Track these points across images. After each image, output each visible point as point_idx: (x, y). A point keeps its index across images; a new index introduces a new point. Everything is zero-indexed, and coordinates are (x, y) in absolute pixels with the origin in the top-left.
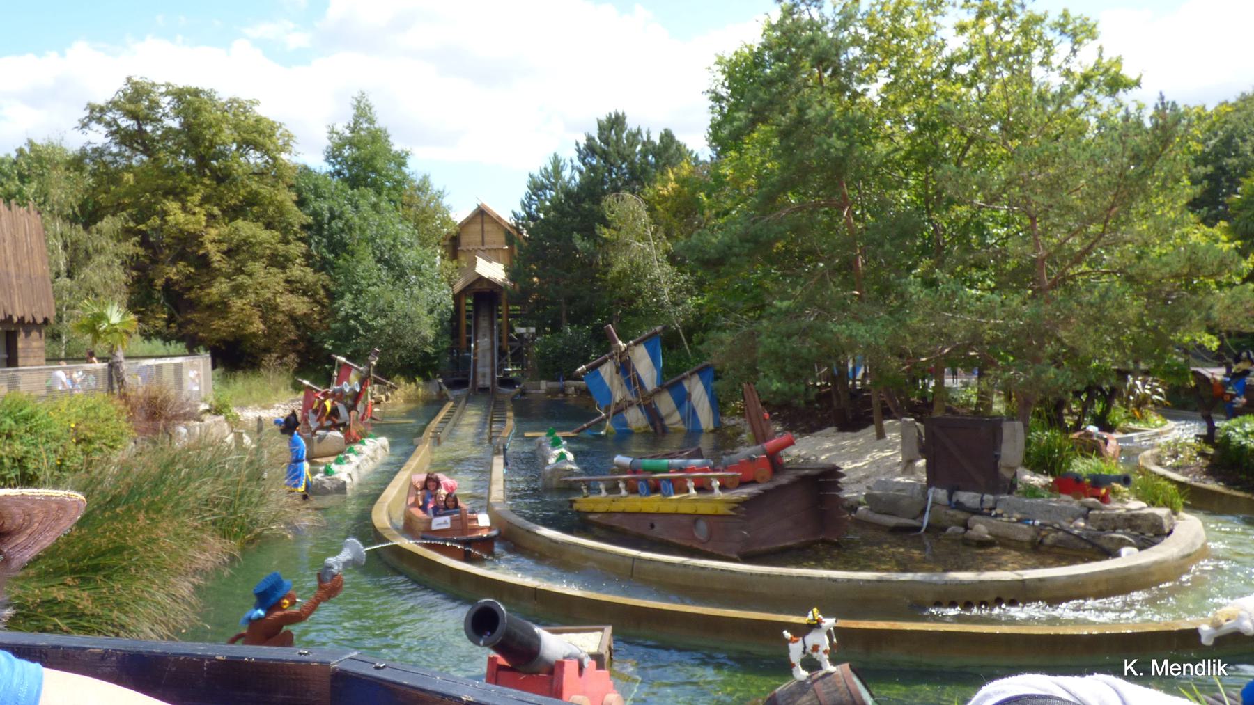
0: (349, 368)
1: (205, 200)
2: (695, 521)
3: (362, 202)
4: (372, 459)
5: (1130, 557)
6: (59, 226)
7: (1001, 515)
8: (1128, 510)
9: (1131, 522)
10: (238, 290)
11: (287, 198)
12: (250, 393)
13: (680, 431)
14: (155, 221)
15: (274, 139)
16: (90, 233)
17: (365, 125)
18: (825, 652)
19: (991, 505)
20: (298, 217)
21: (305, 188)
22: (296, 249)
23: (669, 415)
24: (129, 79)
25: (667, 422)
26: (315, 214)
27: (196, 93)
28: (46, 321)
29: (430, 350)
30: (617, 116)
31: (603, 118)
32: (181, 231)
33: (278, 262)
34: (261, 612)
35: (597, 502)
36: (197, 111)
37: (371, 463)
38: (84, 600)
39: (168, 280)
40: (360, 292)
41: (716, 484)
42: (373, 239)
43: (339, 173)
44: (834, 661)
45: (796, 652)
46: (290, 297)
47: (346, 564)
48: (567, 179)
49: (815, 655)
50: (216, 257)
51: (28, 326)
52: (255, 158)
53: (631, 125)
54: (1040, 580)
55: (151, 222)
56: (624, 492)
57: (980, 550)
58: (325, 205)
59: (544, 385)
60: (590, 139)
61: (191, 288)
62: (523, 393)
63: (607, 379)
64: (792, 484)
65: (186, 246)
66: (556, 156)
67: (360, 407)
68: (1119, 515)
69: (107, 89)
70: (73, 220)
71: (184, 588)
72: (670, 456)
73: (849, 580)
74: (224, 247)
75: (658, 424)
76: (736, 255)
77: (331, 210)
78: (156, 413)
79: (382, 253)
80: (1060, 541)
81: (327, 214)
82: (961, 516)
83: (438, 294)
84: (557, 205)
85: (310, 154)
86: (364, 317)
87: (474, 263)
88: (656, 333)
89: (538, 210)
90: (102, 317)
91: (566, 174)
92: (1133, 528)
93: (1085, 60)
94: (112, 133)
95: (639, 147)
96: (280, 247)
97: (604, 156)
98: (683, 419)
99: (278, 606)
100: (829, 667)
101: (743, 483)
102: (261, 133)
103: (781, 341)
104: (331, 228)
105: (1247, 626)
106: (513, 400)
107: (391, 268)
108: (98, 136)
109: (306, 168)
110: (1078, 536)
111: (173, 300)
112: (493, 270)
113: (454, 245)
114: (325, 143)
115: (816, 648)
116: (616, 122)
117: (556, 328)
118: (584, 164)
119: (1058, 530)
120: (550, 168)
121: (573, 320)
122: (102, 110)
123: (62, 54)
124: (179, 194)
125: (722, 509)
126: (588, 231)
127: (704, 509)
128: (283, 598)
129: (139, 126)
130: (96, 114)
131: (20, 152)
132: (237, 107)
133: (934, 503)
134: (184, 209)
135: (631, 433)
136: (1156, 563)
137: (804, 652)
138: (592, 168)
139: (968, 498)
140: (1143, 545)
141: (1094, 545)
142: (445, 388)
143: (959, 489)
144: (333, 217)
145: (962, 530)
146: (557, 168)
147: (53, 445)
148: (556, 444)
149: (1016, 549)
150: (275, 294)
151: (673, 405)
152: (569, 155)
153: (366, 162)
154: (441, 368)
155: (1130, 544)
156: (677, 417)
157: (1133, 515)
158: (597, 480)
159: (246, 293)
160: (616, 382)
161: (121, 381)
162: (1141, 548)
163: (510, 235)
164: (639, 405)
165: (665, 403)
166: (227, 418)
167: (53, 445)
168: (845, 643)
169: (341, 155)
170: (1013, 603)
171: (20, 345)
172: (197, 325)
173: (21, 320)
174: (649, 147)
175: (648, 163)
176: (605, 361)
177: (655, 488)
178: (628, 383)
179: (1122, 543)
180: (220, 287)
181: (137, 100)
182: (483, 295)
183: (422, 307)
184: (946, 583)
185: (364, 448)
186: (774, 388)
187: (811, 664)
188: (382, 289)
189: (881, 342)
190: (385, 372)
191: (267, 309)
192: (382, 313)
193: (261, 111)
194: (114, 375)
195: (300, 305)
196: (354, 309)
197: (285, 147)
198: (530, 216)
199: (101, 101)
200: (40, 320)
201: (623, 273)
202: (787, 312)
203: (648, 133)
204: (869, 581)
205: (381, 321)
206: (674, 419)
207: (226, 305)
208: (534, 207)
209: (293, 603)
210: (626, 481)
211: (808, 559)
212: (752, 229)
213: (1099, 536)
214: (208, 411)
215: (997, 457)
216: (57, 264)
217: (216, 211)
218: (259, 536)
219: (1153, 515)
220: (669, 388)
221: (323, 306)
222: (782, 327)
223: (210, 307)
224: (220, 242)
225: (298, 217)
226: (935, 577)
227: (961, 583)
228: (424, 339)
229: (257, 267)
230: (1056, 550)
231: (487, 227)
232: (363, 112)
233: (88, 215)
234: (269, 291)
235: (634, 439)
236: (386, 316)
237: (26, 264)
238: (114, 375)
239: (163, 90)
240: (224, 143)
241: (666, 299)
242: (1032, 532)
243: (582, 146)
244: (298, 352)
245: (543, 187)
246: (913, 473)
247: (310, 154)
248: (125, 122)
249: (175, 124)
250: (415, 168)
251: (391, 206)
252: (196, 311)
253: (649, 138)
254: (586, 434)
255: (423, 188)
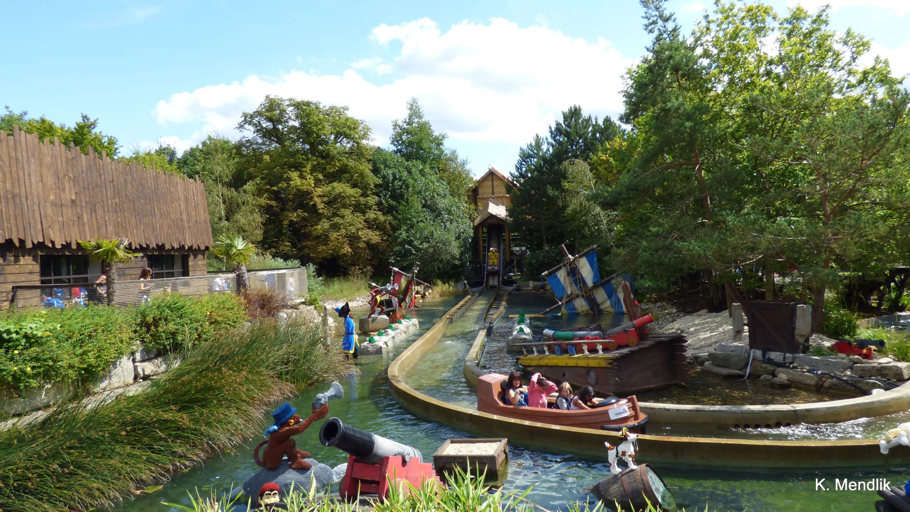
0: (401, 275)
1: (313, 170)
2: (588, 372)
3: (413, 170)
4: (405, 332)
5: (878, 395)
6: (220, 189)
7: (796, 367)
8: (880, 364)
9: (882, 372)
10: (336, 227)
11: (366, 168)
12: (342, 291)
13: (610, 313)
14: (283, 185)
15: (357, 130)
16: (239, 193)
17: (416, 120)
18: (630, 456)
19: (790, 360)
20: (373, 180)
21: (377, 160)
22: (372, 200)
23: (603, 303)
24: (267, 97)
25: (602, 307)
26: (384, 177)
27: (308, 104)
28: (207, 248)
29: (457, 262)
30: (576, 109)
31: (566, 110)
32: (299, 190)
33: (360, 208)
34: (275, 427)
35: (531, 359)
36: (308, 115)
37: (404, 335)
38: (184, 419)
39: (291, 221)
40: (412, 227)
41: (600, 347)
42: (420, 192)
43: (400, 151)
44: (637, 462)
45: (612, 455)
46: (370, 232)
47: (330, 398)
48: (545, 150)
49: (624, 458)
50: (320, 206)
51: (196, 252)
52: (347, 145)
53: (585, 114)
54: (807, 410)
55: (280, 185)
56: (547, 353)
57: (785, 390)
58: (390, 172)
59: (531, 284)
60: (558, 124)
61: (306, 226)
62: (518, 289)
63: (562, 280)
64: (651, 347)
65: (302, 199)
66: (537, 136)
67: (408, 300)
68: (873, 367)
69: (255, 103)
70: (229, 185)
71: (258, 414)
72: (581, 329)
73: (678, 410)
74: (325, 199)
75: (596, 309)
76: (624, 199)
77: (394, 174)
78: (267, 305)
79: (426, 201)
80: (834, 385)
81: (391, 178)
82: (770, 368)
83: (462, 228)
84: (538, 168)
85: (381, 140)
86: (416, 243)
87: (487, 206)
88: (593, 249)
89: (526, 171)
90: (231, 246)
91: (545, 147)
92: (883, 376)
93: (865, 62)
94: (258, 131)
95: (590, 129)
96: (361, 199)
97: (567, 134)
98: (611, 304)
99: (287, 423)
100: (633, 466)
101: (620, 347)
102: (349, 127)
103: (652, 254)
104: (393, 186)
105: (905, 441)
106: (510, 294)
107: (433, 211)
108: (249, 133)
109: (379, 148)
110: (846, 381)
111: (290, 232)
112: (499, 210)
113: (475, 194)
114: (391, 132)
115: (624, 453)
116: (574, 113)
117: (540, 247)
118: (555, 140)
119: (833, 377)
120: (534, 144)
121: (549, 241)
122: (252, 117)
123: (241, 84)
124: (298, 167)
125: (604, 364)
126: (557, 185)
127: (593, 364)
128: (290, 419)
129: (274, 125)
130: (248, 119)
131: (204, 144)
132: (333, 112)
133: (754, 359)
134: (302, 177)
135: (578, 314)
136: (893, 399)
137: (617, 456)
138: (560, 143)
139: (775, 356)
140: (888, 387)
141: (856, 387)
142: (468, 286)
143: (769, 350)
144: (395, 179)
145: (770, 377)
146: (538, 145)
147: (195, 325)
148: (521, 321)
149: (806, 390)
150: (358, 230)
151: (606, 296)
152: (545, 134)
153: (417, 144)
154: (469, 273)
155: (880, 387)
156: (608, 303)
157: (882, 367)
158: (581, 344)
159: (339, 229)
160: (568, 281)
161: (245, 286)
162: (886, 389)
163: (509, 187)
164: (583, 296)
165: (601, 296)
166: (315, 308)
167: (195, 325)
168: (644, 451)
169: (401, 139)
170: (788, 425)
171: (190, 264)
172: (309, 249)
173: (191, 248)
174: (596, 128)
175: (596, 139)
176: (560, 268)
177: (565, 351)
178: (575, 282)
179: (875, 386)
180: (324, 225)
181: (272, 110)
182: (492, 225)
183: (451, 235)
184: (742, 412)
185: (400, 326)
186: (647, 285)
187: (622, 463)
188: (427, 225)
189: (709, 254)
190: (427, 278)
191: (353, 239)
192: (426, 240)
193: (349, 114)
194: (240, 283)
195: (374, 237)
196: (408, 237)
197: (365, 136)
198: (522, 175)
199: (251, 111)
200: (203, 248)
201: (575, 212)
202: (657, 235)
203: (596, 119)
204: (690, 411)
205: (426, 245)
206: (607, 305)
207: (327, 236)
208: (524, 169)
209: (297, 422)
210: (548, 346)
211: (707, 394)
212: (635, 182)
213: (859, 382)
214: (303, 303)
215: (794, 329)
216: (220, 213)
217: (321, 177)
218: (317, 381)
219: (896, 367)
220: (603, 285)
221: (389, 236)
222: (653, 245)
223: (318, 237)
224: (324, 196)
225: (373, 180)
226: (734, 408)
227: (753, 412)
228: (453, 257)
229: (347, 212)
230: (832, 391)
231: (496, 183)
232: (415, 111)
233: (237, 181)
234: (355, 227)
235: (580, 319)
236: (428, 242)
237: (193, 213)
238: (240, 283)
239: (287, 103)
240: (325, 135)
241: (604, 227)
242: (816, 379)
243: (553, 129)
244: (372, 265)
245: (529, 156)
246: (740, 340)
247: (381, 140)
248: (266, 124)
249: (296, 124)
250: (448, 146)
251: (432, 172)
252: (308, 240)
253: (596, 122)
254: (548, 316)
255: (453, 158)
